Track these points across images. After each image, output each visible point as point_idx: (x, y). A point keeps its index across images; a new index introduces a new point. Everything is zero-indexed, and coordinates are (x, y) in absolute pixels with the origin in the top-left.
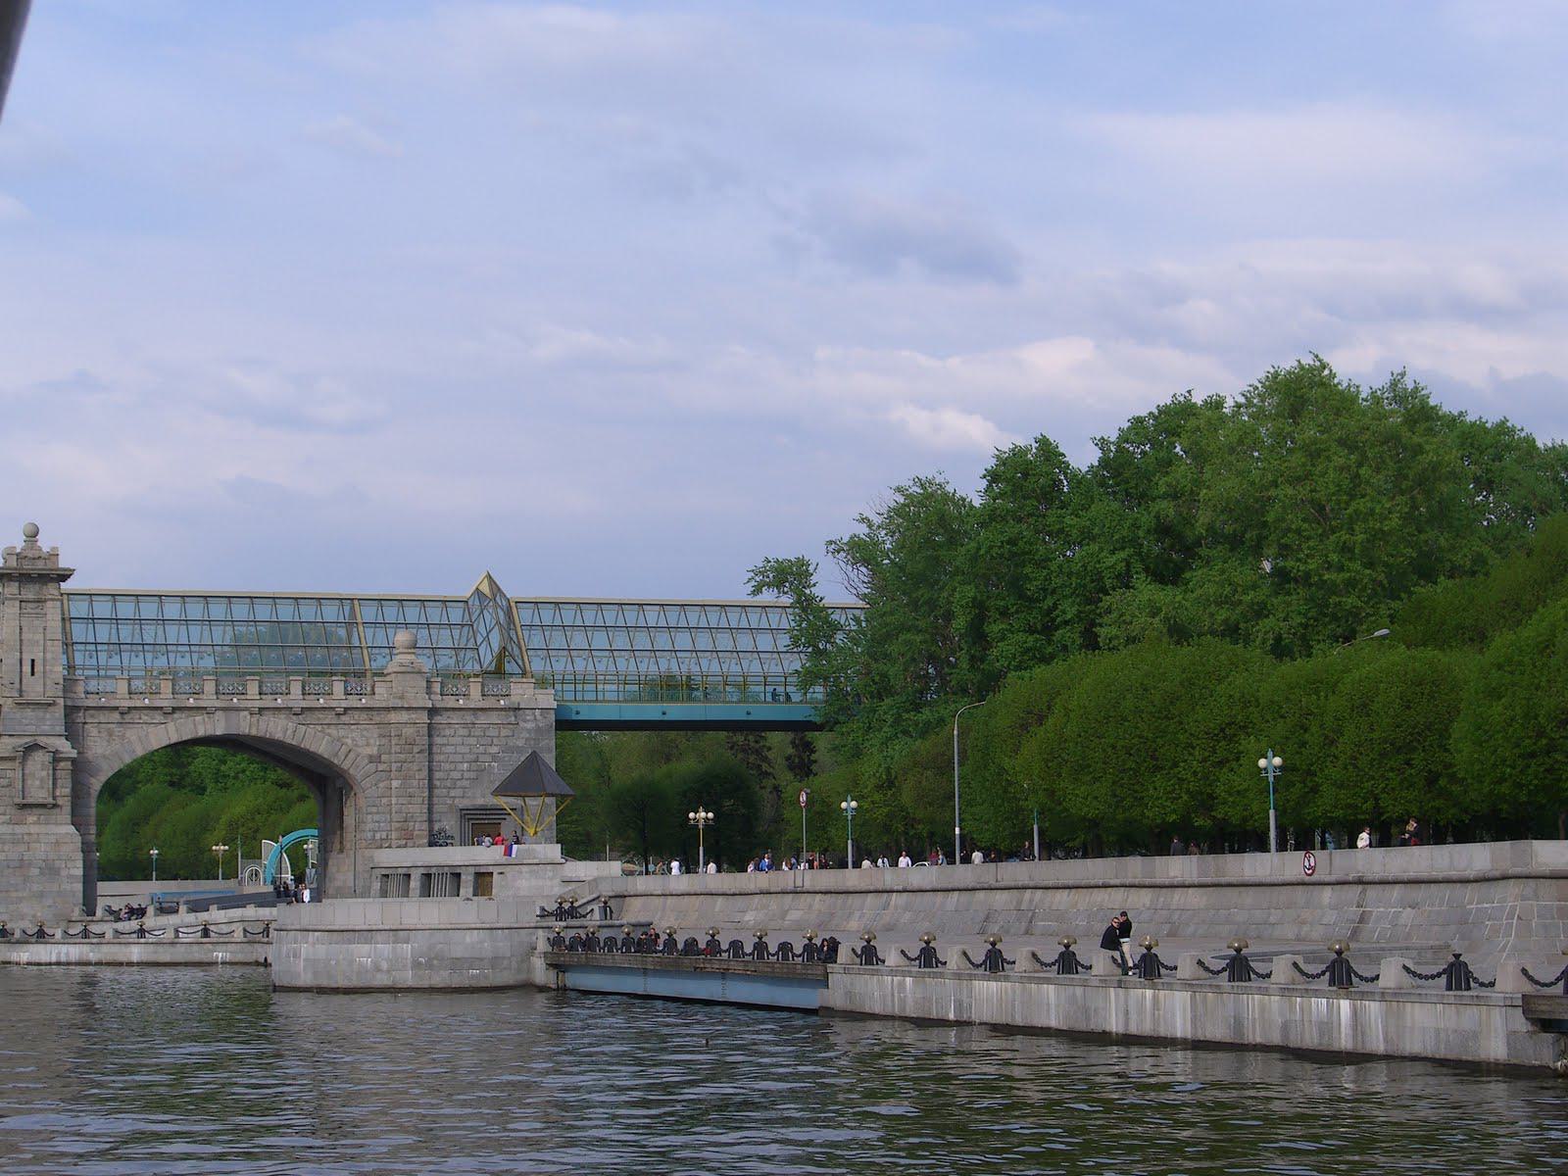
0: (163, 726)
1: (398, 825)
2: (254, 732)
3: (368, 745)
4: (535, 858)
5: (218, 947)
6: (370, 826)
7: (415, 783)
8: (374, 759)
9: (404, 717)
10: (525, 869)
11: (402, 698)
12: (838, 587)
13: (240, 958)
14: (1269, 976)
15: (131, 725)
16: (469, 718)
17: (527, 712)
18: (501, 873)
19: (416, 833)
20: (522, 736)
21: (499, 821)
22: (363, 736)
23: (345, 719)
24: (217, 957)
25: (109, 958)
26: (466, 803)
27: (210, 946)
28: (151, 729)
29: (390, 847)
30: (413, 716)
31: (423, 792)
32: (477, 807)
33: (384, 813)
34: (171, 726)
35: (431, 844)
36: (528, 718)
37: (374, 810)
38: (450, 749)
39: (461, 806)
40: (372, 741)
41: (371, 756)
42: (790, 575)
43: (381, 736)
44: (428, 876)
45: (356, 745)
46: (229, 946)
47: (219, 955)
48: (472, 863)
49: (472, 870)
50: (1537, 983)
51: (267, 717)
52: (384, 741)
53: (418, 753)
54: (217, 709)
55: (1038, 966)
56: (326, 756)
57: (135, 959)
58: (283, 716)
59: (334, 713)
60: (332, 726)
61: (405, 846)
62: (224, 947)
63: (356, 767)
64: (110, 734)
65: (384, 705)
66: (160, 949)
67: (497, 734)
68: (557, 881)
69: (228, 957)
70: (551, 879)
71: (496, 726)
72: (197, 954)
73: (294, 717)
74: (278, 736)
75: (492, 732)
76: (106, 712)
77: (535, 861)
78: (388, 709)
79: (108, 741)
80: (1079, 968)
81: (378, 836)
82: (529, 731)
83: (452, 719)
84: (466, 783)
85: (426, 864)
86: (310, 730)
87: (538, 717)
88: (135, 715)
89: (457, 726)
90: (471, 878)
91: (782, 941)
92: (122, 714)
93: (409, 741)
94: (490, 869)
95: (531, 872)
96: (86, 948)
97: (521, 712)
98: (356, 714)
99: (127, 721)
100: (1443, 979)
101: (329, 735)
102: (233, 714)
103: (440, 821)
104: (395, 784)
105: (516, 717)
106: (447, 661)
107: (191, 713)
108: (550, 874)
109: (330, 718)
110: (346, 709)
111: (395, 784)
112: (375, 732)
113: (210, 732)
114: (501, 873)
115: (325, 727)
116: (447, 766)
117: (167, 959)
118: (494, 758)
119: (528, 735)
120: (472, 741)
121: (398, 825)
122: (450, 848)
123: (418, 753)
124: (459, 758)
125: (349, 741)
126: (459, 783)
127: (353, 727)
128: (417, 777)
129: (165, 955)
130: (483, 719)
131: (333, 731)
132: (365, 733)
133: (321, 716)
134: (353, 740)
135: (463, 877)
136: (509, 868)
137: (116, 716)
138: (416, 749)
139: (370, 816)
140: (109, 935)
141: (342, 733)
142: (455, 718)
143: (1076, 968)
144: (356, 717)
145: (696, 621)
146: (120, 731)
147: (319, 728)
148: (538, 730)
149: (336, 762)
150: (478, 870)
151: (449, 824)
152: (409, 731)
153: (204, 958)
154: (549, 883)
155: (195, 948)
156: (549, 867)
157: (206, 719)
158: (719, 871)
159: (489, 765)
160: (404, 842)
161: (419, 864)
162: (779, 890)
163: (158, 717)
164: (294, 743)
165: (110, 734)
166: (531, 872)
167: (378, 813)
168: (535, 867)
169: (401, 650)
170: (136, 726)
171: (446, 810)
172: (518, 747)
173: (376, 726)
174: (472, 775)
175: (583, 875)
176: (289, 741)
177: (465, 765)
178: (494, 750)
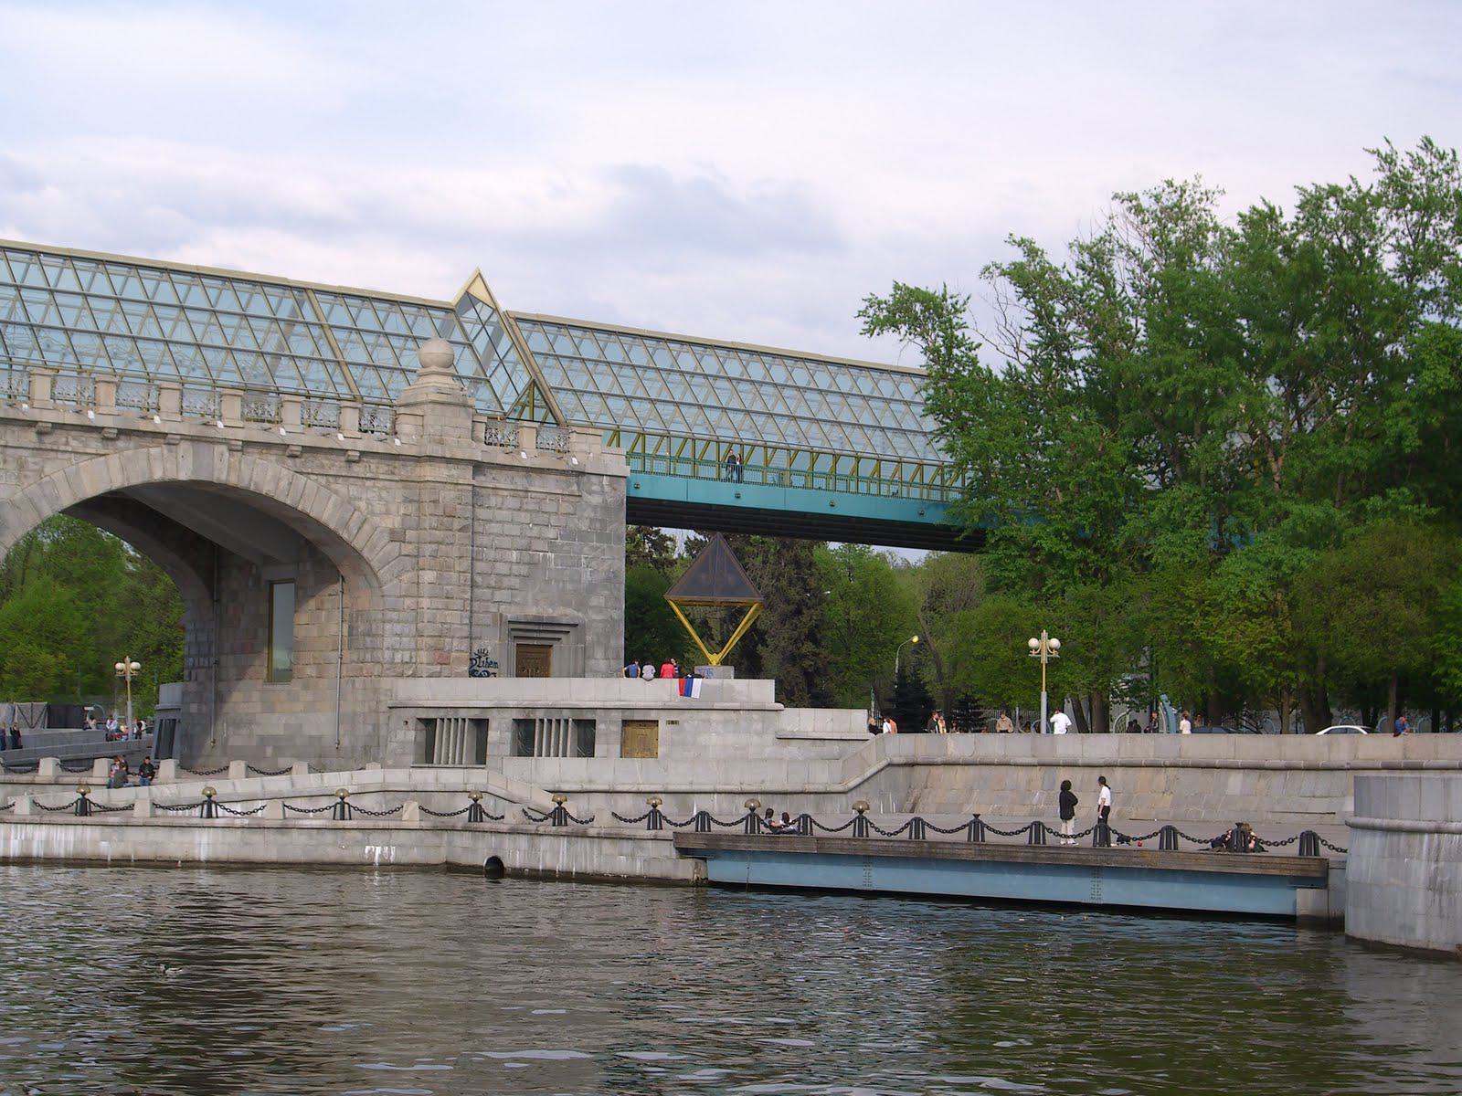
0: (102, 459)
1: (430, 641)
2: (233, 480)
3: (388, 513)
4: (735, 701)
5: (375, 836)
6: (388, 642)
7: (454, 575)
8: (396, 536)
9: (442, 472)
10: (714, 716)
11: (441, 442)
12: (999, 337)
13: (415, 855)
14: (131, 807)
15: (52, 455)
16: (520, 481)
17: (594, 479)
18: (673, 722)
19: (454, 654)
20: (586, 515)
21: (557, 636)
22: (381, 499)
23: (358, 469)
24: (372, 854)
25: (146, 852)
26: (512, 613)
27: (358, 835)
28: (85, 463)
29: (414, 675)
30: (454, 472)
31: (464, 592)
32: (530, 619)
33: (407, 622)
34: (114, 460)
35: (472, 674)
36: (594, 488)
37: (394, 615)
38: (495, 528)
39: (510, 617)
40: (393, 508)
41: (392, 532)
42: (913, 310)
43: (407, 500)
44: (429, 723)
45: (373, 513)
46: (395, 834)
47: (377, 851)
48: (618, 704)
49: (618, 716)
50: (676, 825)
51: (253, 456)
52: (412, 508)
53: (460, 530)
54: (184, 437)
55: (525, 819)
56: (332, 526)
57: (203, 854)
58: (273, 458)
59: (343, 459)
60: (340, 480)
61: (439, 675)
62: (384, 836)
63: (377, 550)
64: (22, 466)
65: (413, 451)
66: (256, 837)
67: (555, 510)
68: (770, 738)
69: (393, 855)
70: (759, 734)
71: (553, 497)
72: (331, 849)
73: (290, 462)
74: (267, 488)
75: (550, 506)
76: (16, 429)
77: (736, 705)
78: (417, 459)
79: (18, 478)
80: (569, 820)
81: (398, 658)
82: (595, 508)
83: (499, 481)
84: (515, 582)
85: (525, 704)
86: (311, 483)
87: (607, 489)
88: (59, 438)
89: (506, 493)
90: (617, 728)
91: (703, 809)
92: (40, 433)
93: (448, 511)
94: (653, 716)
95: (726, 722)
96: (90, 834)
97: (585, 478)
98: (373, 463)
99: (49, 447)
100: (550, 821)
101: (336, 492)
102: (203, 447)
103: (480, 638)
104: (429, 576)
105: (578, 485)
106: (255, 371)
107: (143, 441)
108: (759, 726)
109: (337, 465)
110: (363, 453)
111: (429, 576)
112: (398, 492)
113: (171, 475)
114: (673, 722)
115: (330, 479)
116: (492, 554)
117: (272, 855)
118: (552, 546)
119: (592, 515)
120: (524, 517)
121: (430, 641)
122: (491, 680)
123: (460, 530)
124: (506, 542)
125: (362, 505)
126: (506, 582)
127: (368, 483)
128: (457, 568)
129: (264, 848)
130: (538, 484)
131: (340, 487)
132: (384, 494)
133: (325, 462)
134: (368, 504)
135: (600, 727)
136: (687, 715)
137: (30, 437)
138: (457, 524)
139: (388, 626)
140: (142, 811)
141: (354, 491)
142: (503, 480)
143: (566, 821)
144: (373, 466)
145: (73, 322)
146: (35, 463)
147: (323, 480)
148: (606, 507)
149: (345, 536)
150: (628, 716)
151: (494, 644)
152: (448, 495)
153: (350, 855)
154: (756, 739)
155: (329, 837)
156: (755, 715)
157: (165, 452)
158: (1193, 730)
159: (545, 556)
160: (438, 668)
161: (511, 704)
162: (1282, 763)
163: (94, 445)
164: (288, 502)
165: (22, 466)
166: (726, 722)
167: (398, 622)
168: (733, 715)
169: (433, 368)
170: (59, 455)
171: (489, 622)
172: (580, 531)
173: (400, 485)
174: (524, 570)
175: (810, 729)
176: (282, 499)
177: (515, 553)
178: (551, 533)
